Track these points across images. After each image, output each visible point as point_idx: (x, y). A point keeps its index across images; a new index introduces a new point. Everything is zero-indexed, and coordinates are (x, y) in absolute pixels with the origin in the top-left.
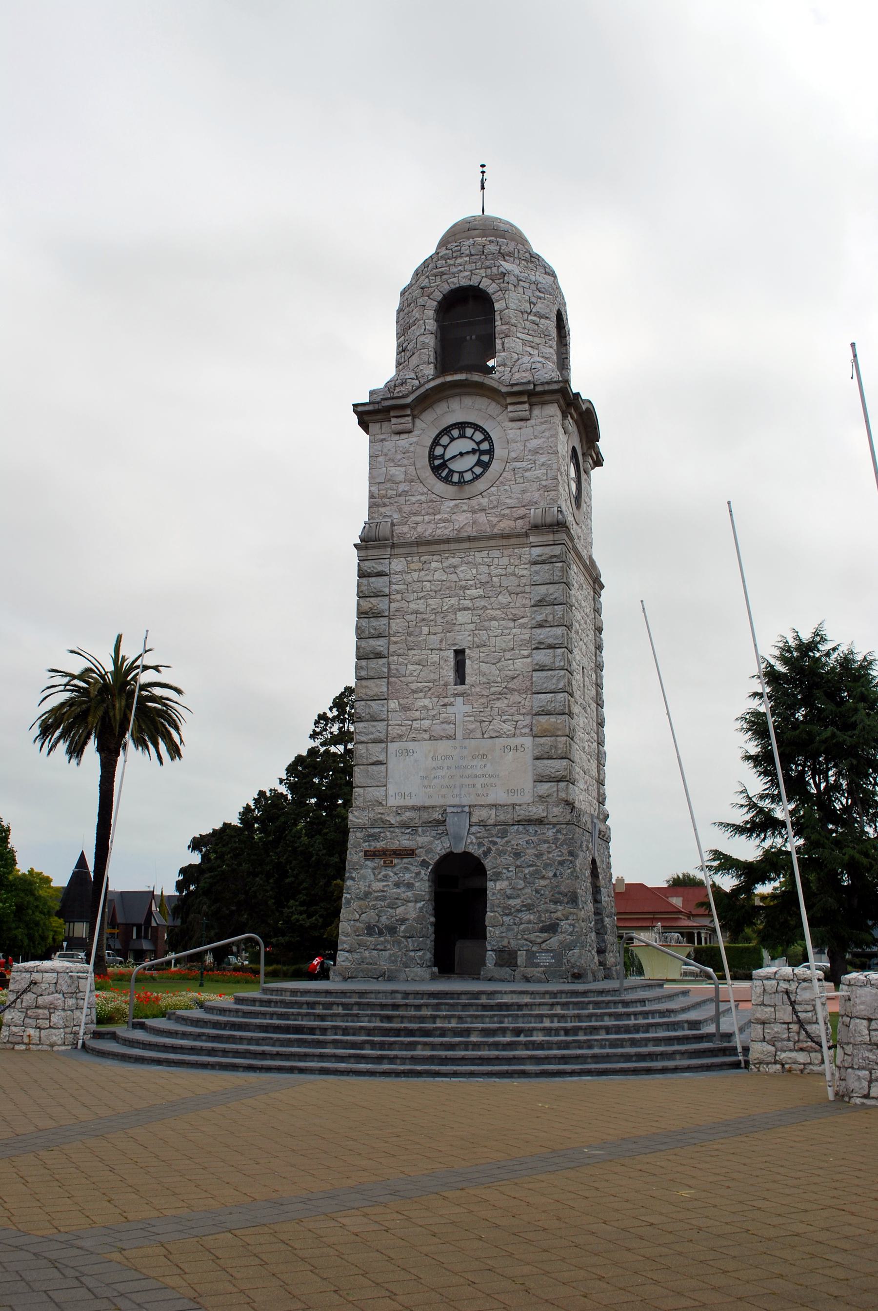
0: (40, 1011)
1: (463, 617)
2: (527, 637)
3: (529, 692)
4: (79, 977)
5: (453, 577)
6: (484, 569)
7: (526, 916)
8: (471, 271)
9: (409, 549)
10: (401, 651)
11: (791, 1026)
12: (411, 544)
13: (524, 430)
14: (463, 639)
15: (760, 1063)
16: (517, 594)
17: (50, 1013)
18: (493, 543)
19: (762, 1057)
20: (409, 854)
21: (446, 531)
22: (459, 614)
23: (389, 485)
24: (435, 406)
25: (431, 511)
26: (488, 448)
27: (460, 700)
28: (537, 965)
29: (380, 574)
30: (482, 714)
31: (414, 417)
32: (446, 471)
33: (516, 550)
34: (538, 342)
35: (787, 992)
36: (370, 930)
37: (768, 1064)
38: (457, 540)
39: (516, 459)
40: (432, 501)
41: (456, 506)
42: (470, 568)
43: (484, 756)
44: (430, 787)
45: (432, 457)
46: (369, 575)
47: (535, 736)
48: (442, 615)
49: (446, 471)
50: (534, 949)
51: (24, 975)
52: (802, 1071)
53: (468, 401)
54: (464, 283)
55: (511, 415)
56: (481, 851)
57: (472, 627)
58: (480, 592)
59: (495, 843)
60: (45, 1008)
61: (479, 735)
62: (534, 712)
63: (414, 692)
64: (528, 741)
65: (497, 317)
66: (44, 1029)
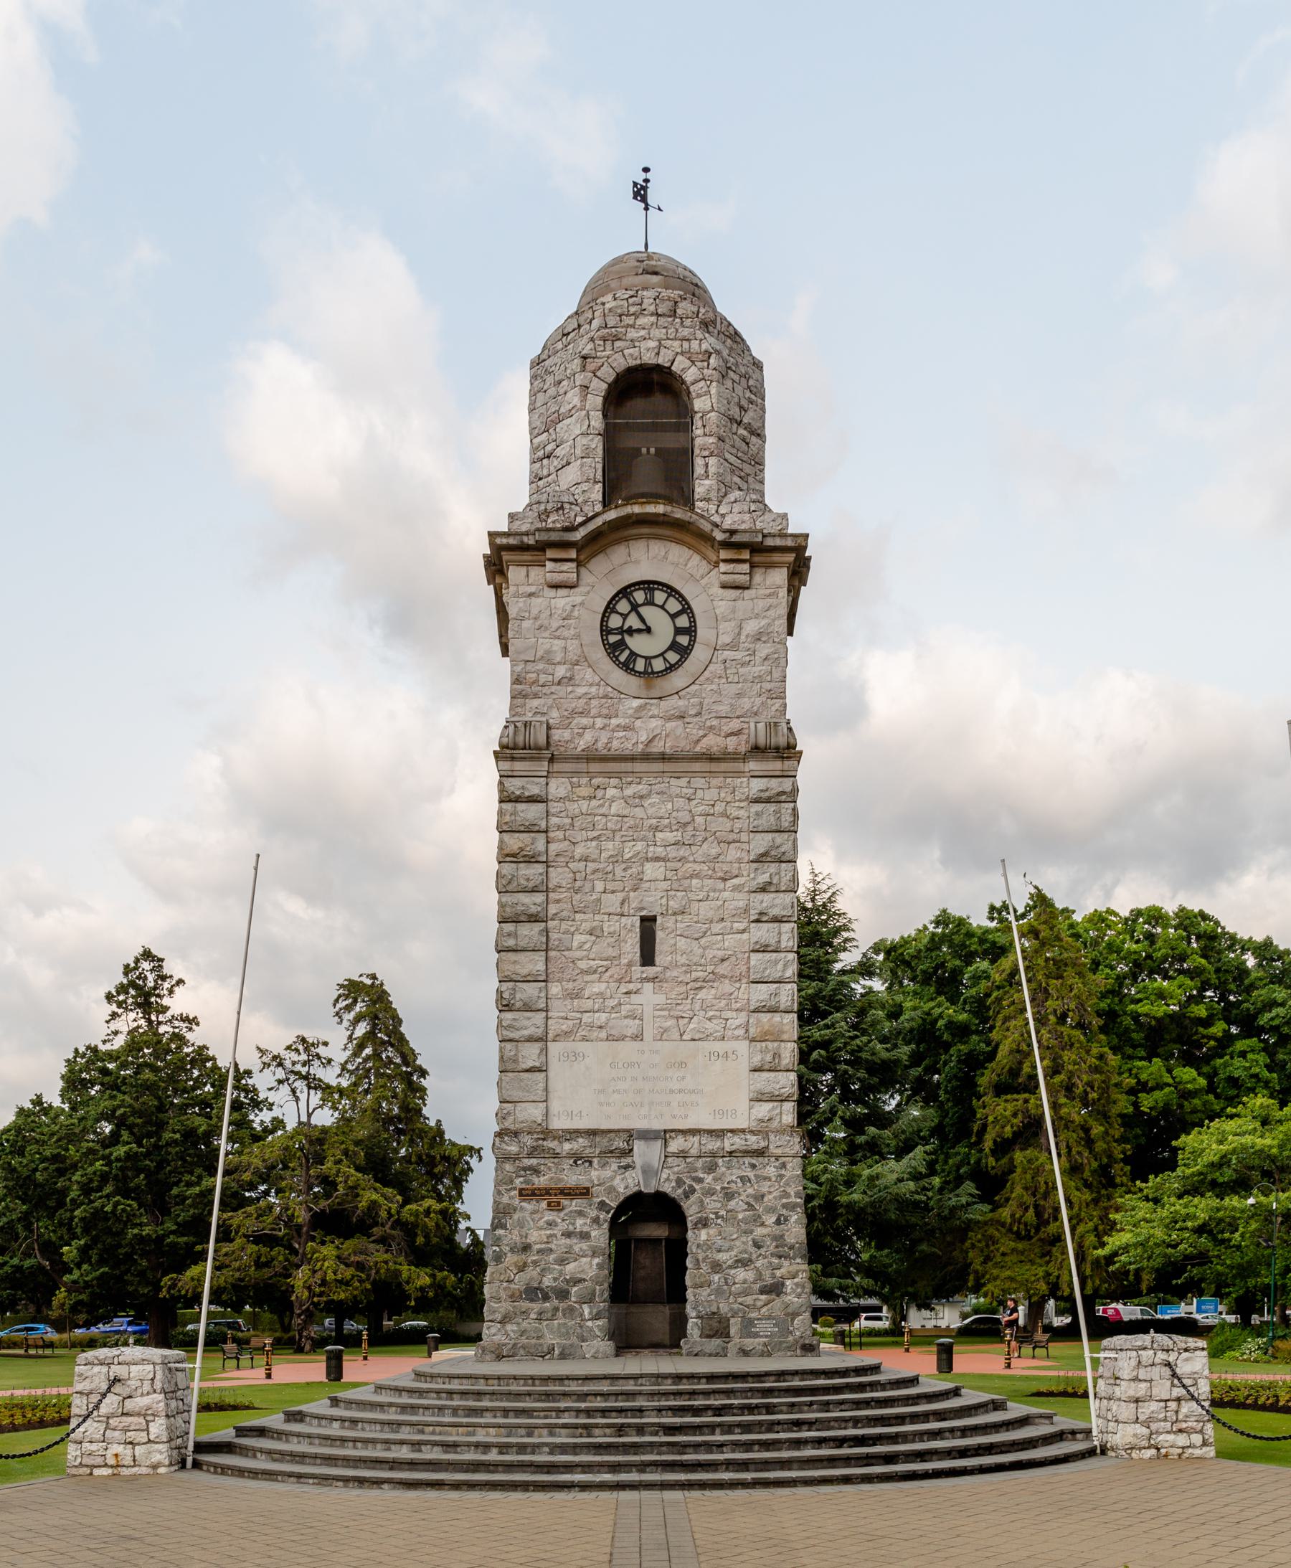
0: (130, 1419)
1: (651, 870)
2: (742, 904)
3: (744, 980)
4: (177, 1370)
5: (639, 812)
6: (680, 802)
7: (741, 1274)
8: (659, 341)
9: (574, 765)
10: (564, 914)
11: (1169, 1404)
12: (577, 759)
13: (740, 603)
14: (652, 901)
15: (1132, 1449)
16: (729, 843)
17: (147, 1422)
18: (697, 766)
19: (1134, 1441)
20: (581, 1194)
21: (635, 742)
22: (648, 866)
23: (540, 666)
24: (608, 551)
25: (605, 711)
26: (687, 625)
27: (649, 986)
28: (756, 1335)
29: (533, 800)
30: (679, 1007)
31: (580, 564)
32: (627, 652)
33: (729, 780)
34: (748, 471)
35: (1168, 1364)
36: (534, 1293)
37: (1140, 1449)
38: (646, 757)
39: (726, 647)
40: (606, 697)
41: (641, 708)
42: (665, 799)
43: (683, 1064)
44: (608, 1104)
45: (605, 630)
46: (518, 800)
47: (753, 1040)
48: (624, 866)
49: (627, 652)
50: (753, 1315)
51: (96, 1369)
52: (1180, 1455)
53: (657, 548)
54: (649, 358)
55: (723, 577)
56: (680, 1191)
57: (665, 885)
58: (677, 836)
59: (700, 1180)
60: (139, 1414)
61: (677, 1036)
62: (752, 1008)
63: (583, 972)
64: (742, 1047)
65: (698, 422)
66: (138, 1444)
